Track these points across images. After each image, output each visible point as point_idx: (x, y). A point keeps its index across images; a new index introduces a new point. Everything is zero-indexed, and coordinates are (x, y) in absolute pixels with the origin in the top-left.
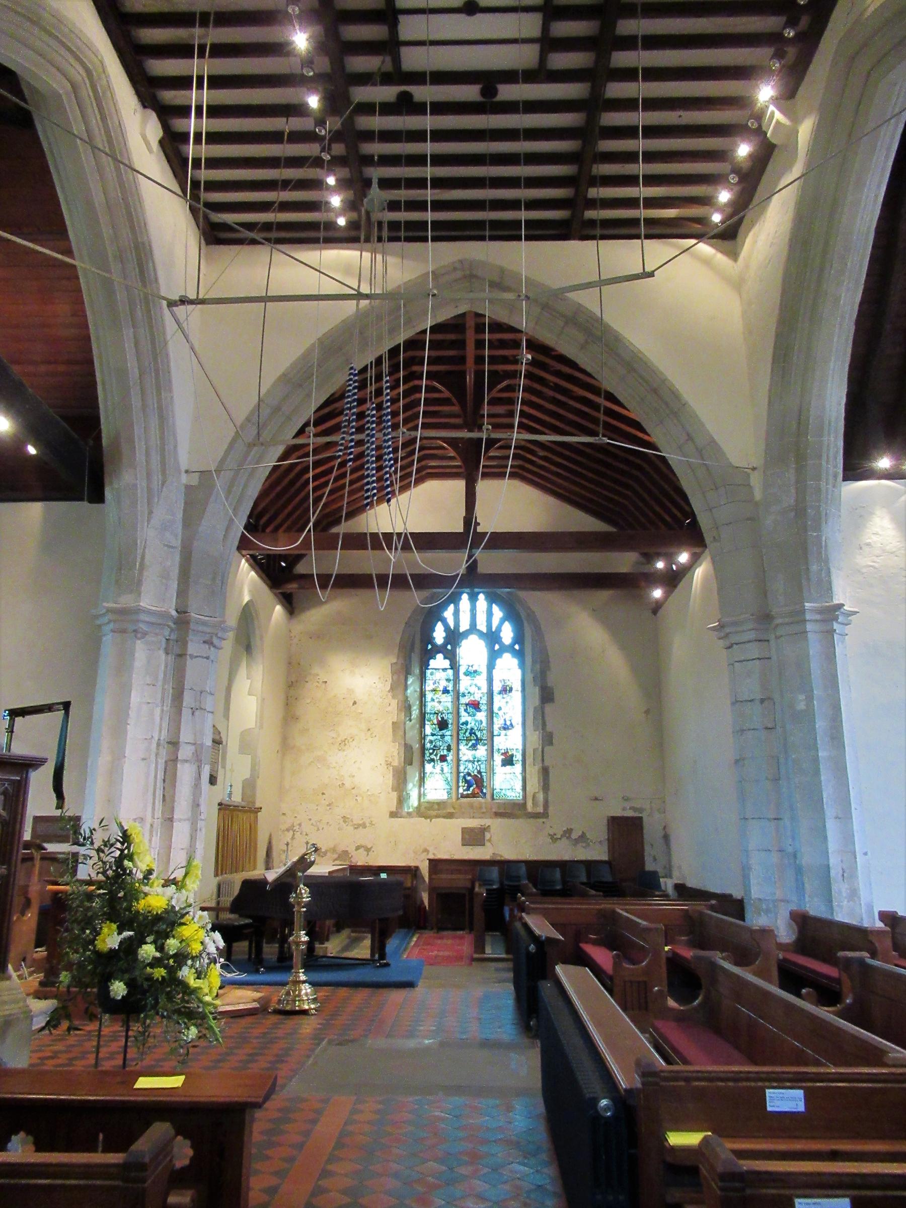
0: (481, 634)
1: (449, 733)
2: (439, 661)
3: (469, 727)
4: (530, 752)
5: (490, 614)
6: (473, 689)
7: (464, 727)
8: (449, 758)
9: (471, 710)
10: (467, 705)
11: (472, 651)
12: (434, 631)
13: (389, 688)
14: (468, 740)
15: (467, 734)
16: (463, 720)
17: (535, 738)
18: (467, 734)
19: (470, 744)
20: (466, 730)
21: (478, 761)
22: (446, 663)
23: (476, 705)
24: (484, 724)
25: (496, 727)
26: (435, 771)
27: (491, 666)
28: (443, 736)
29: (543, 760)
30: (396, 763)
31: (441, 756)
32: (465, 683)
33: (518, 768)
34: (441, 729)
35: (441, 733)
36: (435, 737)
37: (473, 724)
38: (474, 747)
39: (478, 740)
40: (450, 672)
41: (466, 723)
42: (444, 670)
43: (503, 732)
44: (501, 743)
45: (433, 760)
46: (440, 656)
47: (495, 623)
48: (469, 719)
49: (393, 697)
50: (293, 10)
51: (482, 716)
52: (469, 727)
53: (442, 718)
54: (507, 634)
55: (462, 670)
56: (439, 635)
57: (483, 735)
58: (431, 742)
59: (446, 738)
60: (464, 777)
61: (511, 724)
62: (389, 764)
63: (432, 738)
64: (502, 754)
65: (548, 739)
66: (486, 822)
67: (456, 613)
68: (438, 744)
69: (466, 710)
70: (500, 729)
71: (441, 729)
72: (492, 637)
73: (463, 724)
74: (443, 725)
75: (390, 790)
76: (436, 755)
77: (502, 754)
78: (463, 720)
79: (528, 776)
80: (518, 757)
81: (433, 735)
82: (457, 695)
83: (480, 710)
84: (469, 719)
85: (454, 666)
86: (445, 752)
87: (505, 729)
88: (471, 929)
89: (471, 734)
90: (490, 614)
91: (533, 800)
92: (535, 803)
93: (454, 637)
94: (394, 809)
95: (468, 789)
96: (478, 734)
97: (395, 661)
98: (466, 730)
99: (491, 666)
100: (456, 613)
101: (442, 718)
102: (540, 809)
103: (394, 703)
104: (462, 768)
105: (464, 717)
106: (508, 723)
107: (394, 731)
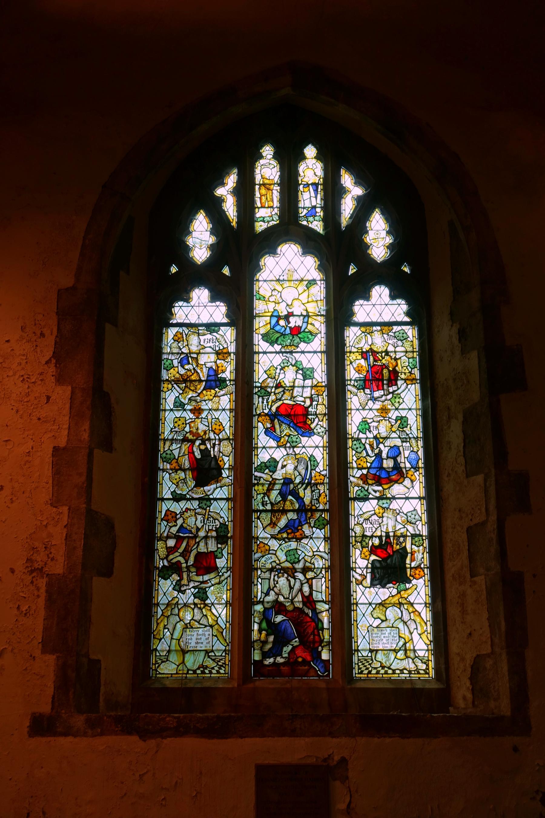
0: (309, 242)
1: (222, 492)
2: (200, 307)
3: (279, 474)
4: (456, 536)
5: (332, 192)
6: (289, 377)
7: (265, 476)
8: (221, 563)
9: (285, 430)
10: (272, 417)
11: (289, 279)
12: (189, 233)
13: (49, 354)
14: (277, 511)
15: (274, 494)
16: (263, 456)
17: (472, 496)
18: (274, 494)
19: (283, 522)
20: (272, 484)
21: (305, 570)
22: (218, 312)
23: (297, 418)
24: (322, 467)
25: (355, 475)
26: (183, 598)
27: (339, 316)
28: (206, 501)
29: (502, 555)
30: (58, 568)
31: (199, 555)
32: (267, 361)
33: (420, 591)
34: (201, 482)
35: (199, 493)
36: (183, 504)
37: (290, 468)
38: (293, 531)
39: (305, 511)
40: (228, 335)
41: (272, 465)
42: (212, 327)
43: (375, 489)
44: (365, 516)
45: (176, 568)
46: (200, 295)
47: (348, 207)
48: (279, 454)
49: (60, 380)
50: (296, 641)
51: (315, 446)
52: (279, 474)
53: (205, 453)
54: (378, 237)
55: (261, 325)
56: (200, 239)
57: (320, 497)
58: (171, 517)
59: (215, 507)
60: (265, 616)
61: (397, 467)
62: (36, 571)
63: (176, 507)
64: (374, 550)
65: (513, 494)
66: (334, 747)
67: (245, 193)
68: (191, 521)
69: (269, 432)
70: (364, 478)
71: (201, 482)
72: (338, 250)
73: (263, 467)
74: (205, 470)
75: (37, 653)
76: (185, 554)
77: (374, 550)
78: (263, 456)
79: (453, 611)
80: (419, 556)
81: (177, 498)
82: (245, 386)
83: (309, 432)
84: (279, 454)
85: (242, 316)
86: (212, 546)
87: (378, 481)
88: (366, 191)
89: (283, 495)
90: (332, 192)
91: (473, 679)
92: (479, 690)
93: (241, 249)
94: (46, 708)
95: (276, 651)
96: (307, 495)
97: (67, 281)
98: (272, 484)
99: (339, 316)
100: (245, 193)
101: (205, 453)
102: (504, 706)
103: (62, 394)
104: (259, 590)
105: (266, 449)
106: (388, 464)
107: (57, 472)
